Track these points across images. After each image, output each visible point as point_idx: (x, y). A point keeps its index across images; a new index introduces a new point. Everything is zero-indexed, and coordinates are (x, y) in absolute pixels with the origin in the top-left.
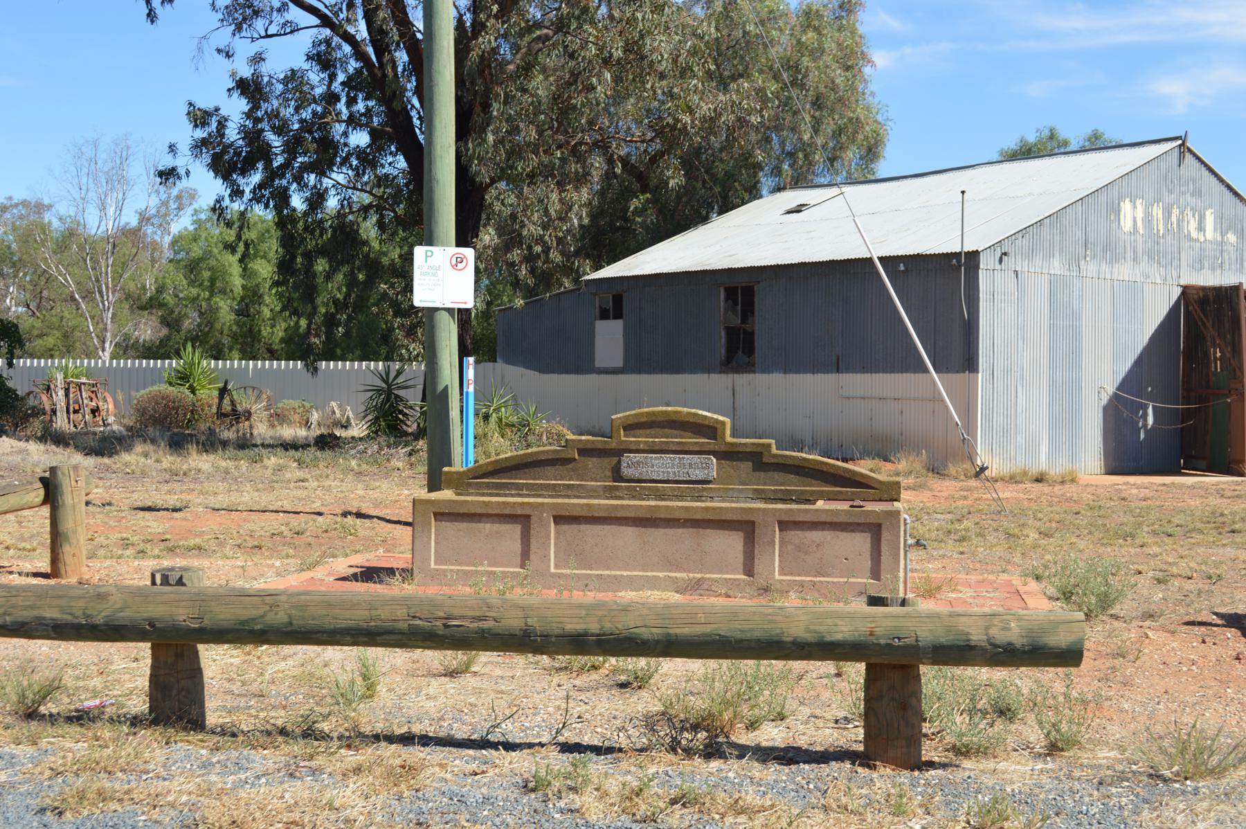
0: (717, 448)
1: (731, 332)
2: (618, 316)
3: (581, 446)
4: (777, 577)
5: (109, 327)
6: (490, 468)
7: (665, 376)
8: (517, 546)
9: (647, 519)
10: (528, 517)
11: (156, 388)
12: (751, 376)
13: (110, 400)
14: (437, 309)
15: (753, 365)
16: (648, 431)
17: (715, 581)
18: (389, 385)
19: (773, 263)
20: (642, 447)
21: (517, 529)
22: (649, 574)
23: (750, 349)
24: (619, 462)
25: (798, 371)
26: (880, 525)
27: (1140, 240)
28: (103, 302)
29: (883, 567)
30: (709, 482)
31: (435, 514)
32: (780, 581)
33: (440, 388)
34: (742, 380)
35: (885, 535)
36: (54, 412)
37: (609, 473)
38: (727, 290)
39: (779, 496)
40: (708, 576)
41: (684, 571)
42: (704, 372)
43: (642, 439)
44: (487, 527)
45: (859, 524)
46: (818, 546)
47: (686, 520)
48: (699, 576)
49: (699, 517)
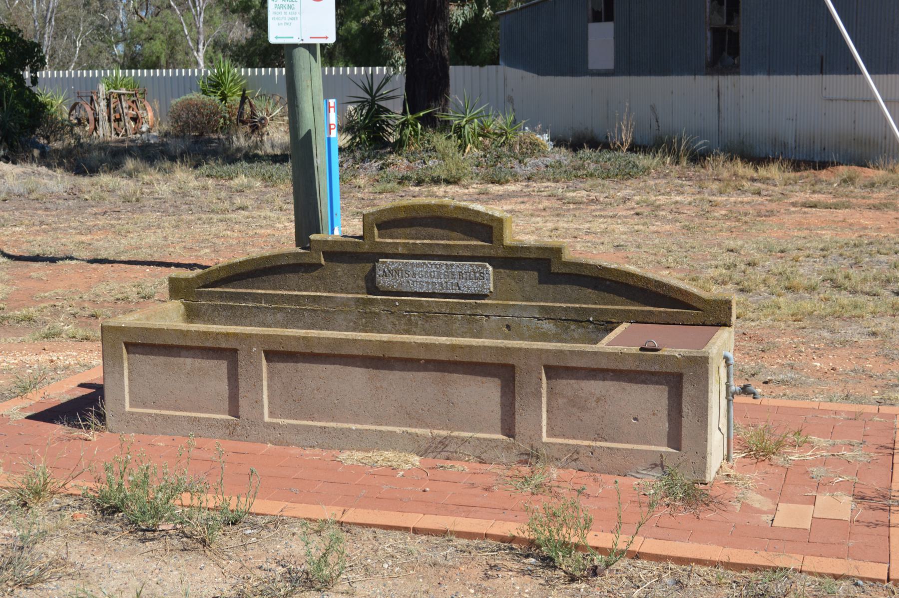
0: (493, 253)
1: (717, 32)
2: (609, 18)
3: (327, 249)
4: (545, 439)
5: (201, 30)
6: (223, 275)
7: (653, 78)
8: (224, 387)
9: (379, 358)
10: (235, 351)
11: (189, 96)
12: (736, 77)
13: (149, 108)
14: (295, 46)
15: (738, 66)
16: (408, 230)
17: (464, 441)
18: (373, 97)
20: (400, 250)
21: (222, 366)
22: (383, 428)
23: (735, 51)
24: (374, 269)
25: (782, 73)
26: (680, 376)
28: (195, 7)
29: (684, 431)
30: (484, 297)
31: (127, 345)
32: (547, 444)
33: (303, 133)
34: (727, 81)
35: (688, 390)
36: (96, 120)
37: (362, 283)
39: (573, 316)
40: (455, 434)
41: (427, 426)
42: (690, 74)
43: (400, 241)
44: (188, 362)
45: (653, 374)
46: (598, 400)
47: (428, 361)
48: (444, 433)
49: (443, 357)
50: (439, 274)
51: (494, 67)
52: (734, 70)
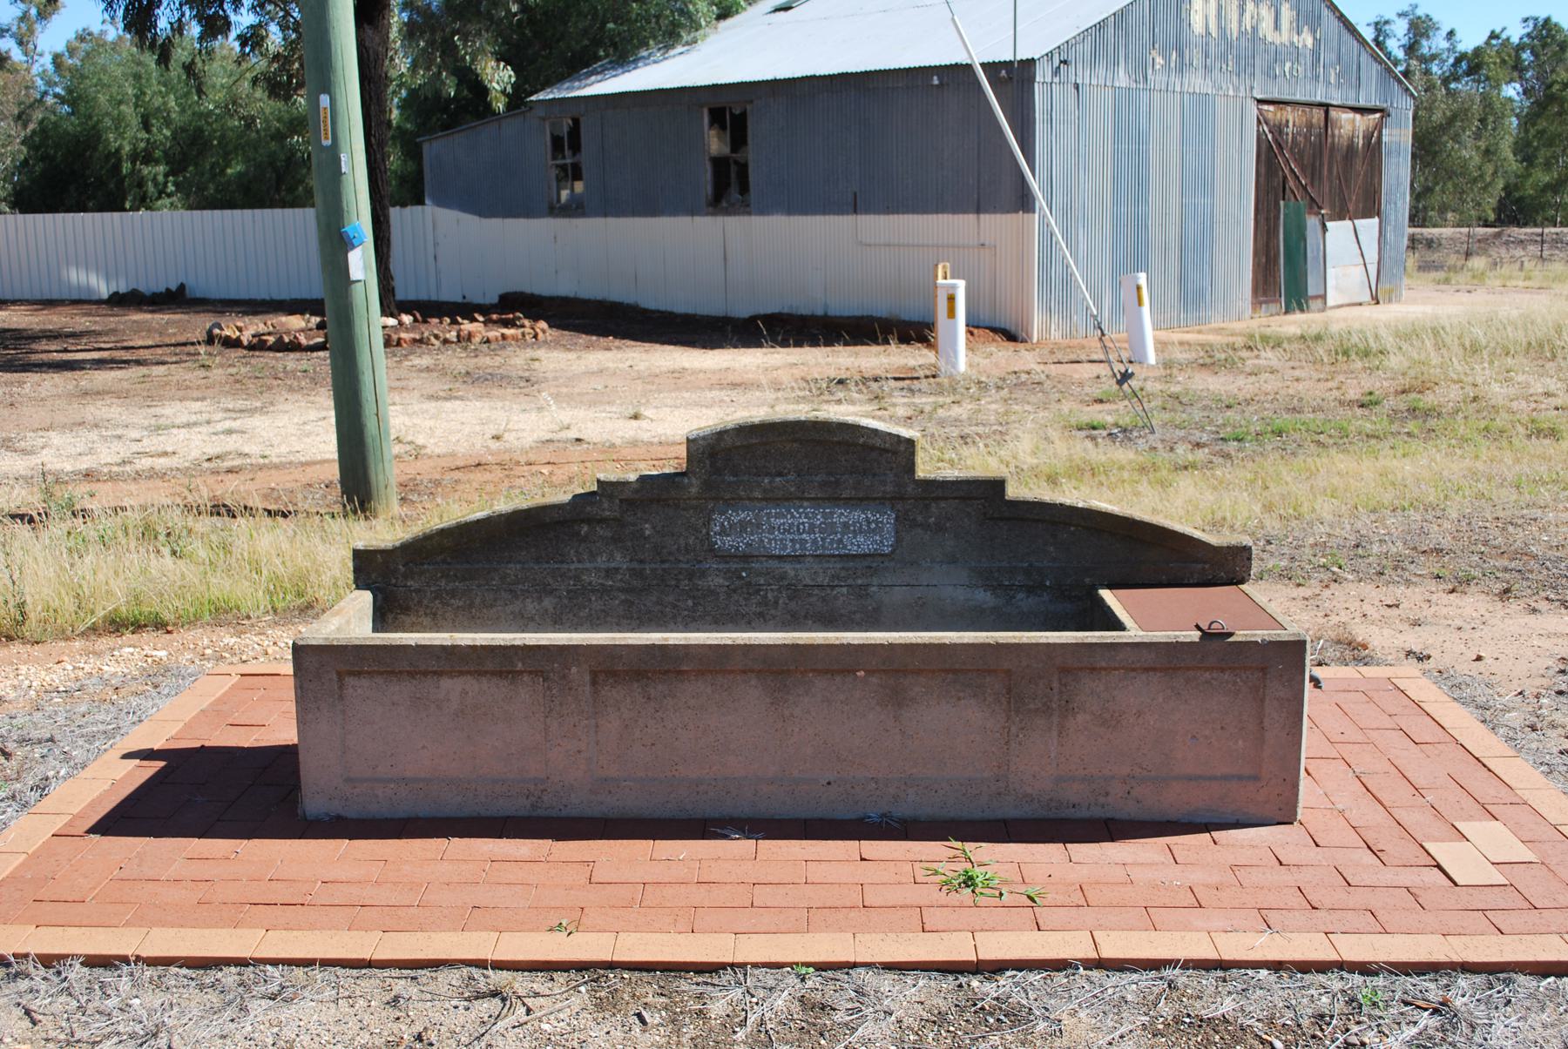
1: (719, 164)
19: (769, 77)
23: (744, 188)
27: (1212, 44)
38: (711, 111)
50: (812, 526)
51: (420, 208)
52: (743, 206)
